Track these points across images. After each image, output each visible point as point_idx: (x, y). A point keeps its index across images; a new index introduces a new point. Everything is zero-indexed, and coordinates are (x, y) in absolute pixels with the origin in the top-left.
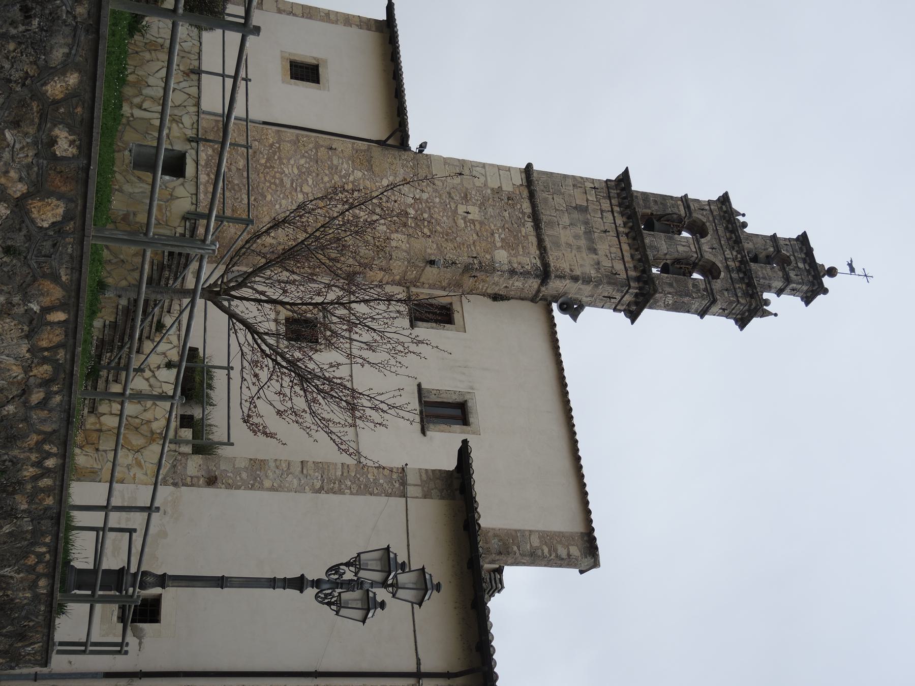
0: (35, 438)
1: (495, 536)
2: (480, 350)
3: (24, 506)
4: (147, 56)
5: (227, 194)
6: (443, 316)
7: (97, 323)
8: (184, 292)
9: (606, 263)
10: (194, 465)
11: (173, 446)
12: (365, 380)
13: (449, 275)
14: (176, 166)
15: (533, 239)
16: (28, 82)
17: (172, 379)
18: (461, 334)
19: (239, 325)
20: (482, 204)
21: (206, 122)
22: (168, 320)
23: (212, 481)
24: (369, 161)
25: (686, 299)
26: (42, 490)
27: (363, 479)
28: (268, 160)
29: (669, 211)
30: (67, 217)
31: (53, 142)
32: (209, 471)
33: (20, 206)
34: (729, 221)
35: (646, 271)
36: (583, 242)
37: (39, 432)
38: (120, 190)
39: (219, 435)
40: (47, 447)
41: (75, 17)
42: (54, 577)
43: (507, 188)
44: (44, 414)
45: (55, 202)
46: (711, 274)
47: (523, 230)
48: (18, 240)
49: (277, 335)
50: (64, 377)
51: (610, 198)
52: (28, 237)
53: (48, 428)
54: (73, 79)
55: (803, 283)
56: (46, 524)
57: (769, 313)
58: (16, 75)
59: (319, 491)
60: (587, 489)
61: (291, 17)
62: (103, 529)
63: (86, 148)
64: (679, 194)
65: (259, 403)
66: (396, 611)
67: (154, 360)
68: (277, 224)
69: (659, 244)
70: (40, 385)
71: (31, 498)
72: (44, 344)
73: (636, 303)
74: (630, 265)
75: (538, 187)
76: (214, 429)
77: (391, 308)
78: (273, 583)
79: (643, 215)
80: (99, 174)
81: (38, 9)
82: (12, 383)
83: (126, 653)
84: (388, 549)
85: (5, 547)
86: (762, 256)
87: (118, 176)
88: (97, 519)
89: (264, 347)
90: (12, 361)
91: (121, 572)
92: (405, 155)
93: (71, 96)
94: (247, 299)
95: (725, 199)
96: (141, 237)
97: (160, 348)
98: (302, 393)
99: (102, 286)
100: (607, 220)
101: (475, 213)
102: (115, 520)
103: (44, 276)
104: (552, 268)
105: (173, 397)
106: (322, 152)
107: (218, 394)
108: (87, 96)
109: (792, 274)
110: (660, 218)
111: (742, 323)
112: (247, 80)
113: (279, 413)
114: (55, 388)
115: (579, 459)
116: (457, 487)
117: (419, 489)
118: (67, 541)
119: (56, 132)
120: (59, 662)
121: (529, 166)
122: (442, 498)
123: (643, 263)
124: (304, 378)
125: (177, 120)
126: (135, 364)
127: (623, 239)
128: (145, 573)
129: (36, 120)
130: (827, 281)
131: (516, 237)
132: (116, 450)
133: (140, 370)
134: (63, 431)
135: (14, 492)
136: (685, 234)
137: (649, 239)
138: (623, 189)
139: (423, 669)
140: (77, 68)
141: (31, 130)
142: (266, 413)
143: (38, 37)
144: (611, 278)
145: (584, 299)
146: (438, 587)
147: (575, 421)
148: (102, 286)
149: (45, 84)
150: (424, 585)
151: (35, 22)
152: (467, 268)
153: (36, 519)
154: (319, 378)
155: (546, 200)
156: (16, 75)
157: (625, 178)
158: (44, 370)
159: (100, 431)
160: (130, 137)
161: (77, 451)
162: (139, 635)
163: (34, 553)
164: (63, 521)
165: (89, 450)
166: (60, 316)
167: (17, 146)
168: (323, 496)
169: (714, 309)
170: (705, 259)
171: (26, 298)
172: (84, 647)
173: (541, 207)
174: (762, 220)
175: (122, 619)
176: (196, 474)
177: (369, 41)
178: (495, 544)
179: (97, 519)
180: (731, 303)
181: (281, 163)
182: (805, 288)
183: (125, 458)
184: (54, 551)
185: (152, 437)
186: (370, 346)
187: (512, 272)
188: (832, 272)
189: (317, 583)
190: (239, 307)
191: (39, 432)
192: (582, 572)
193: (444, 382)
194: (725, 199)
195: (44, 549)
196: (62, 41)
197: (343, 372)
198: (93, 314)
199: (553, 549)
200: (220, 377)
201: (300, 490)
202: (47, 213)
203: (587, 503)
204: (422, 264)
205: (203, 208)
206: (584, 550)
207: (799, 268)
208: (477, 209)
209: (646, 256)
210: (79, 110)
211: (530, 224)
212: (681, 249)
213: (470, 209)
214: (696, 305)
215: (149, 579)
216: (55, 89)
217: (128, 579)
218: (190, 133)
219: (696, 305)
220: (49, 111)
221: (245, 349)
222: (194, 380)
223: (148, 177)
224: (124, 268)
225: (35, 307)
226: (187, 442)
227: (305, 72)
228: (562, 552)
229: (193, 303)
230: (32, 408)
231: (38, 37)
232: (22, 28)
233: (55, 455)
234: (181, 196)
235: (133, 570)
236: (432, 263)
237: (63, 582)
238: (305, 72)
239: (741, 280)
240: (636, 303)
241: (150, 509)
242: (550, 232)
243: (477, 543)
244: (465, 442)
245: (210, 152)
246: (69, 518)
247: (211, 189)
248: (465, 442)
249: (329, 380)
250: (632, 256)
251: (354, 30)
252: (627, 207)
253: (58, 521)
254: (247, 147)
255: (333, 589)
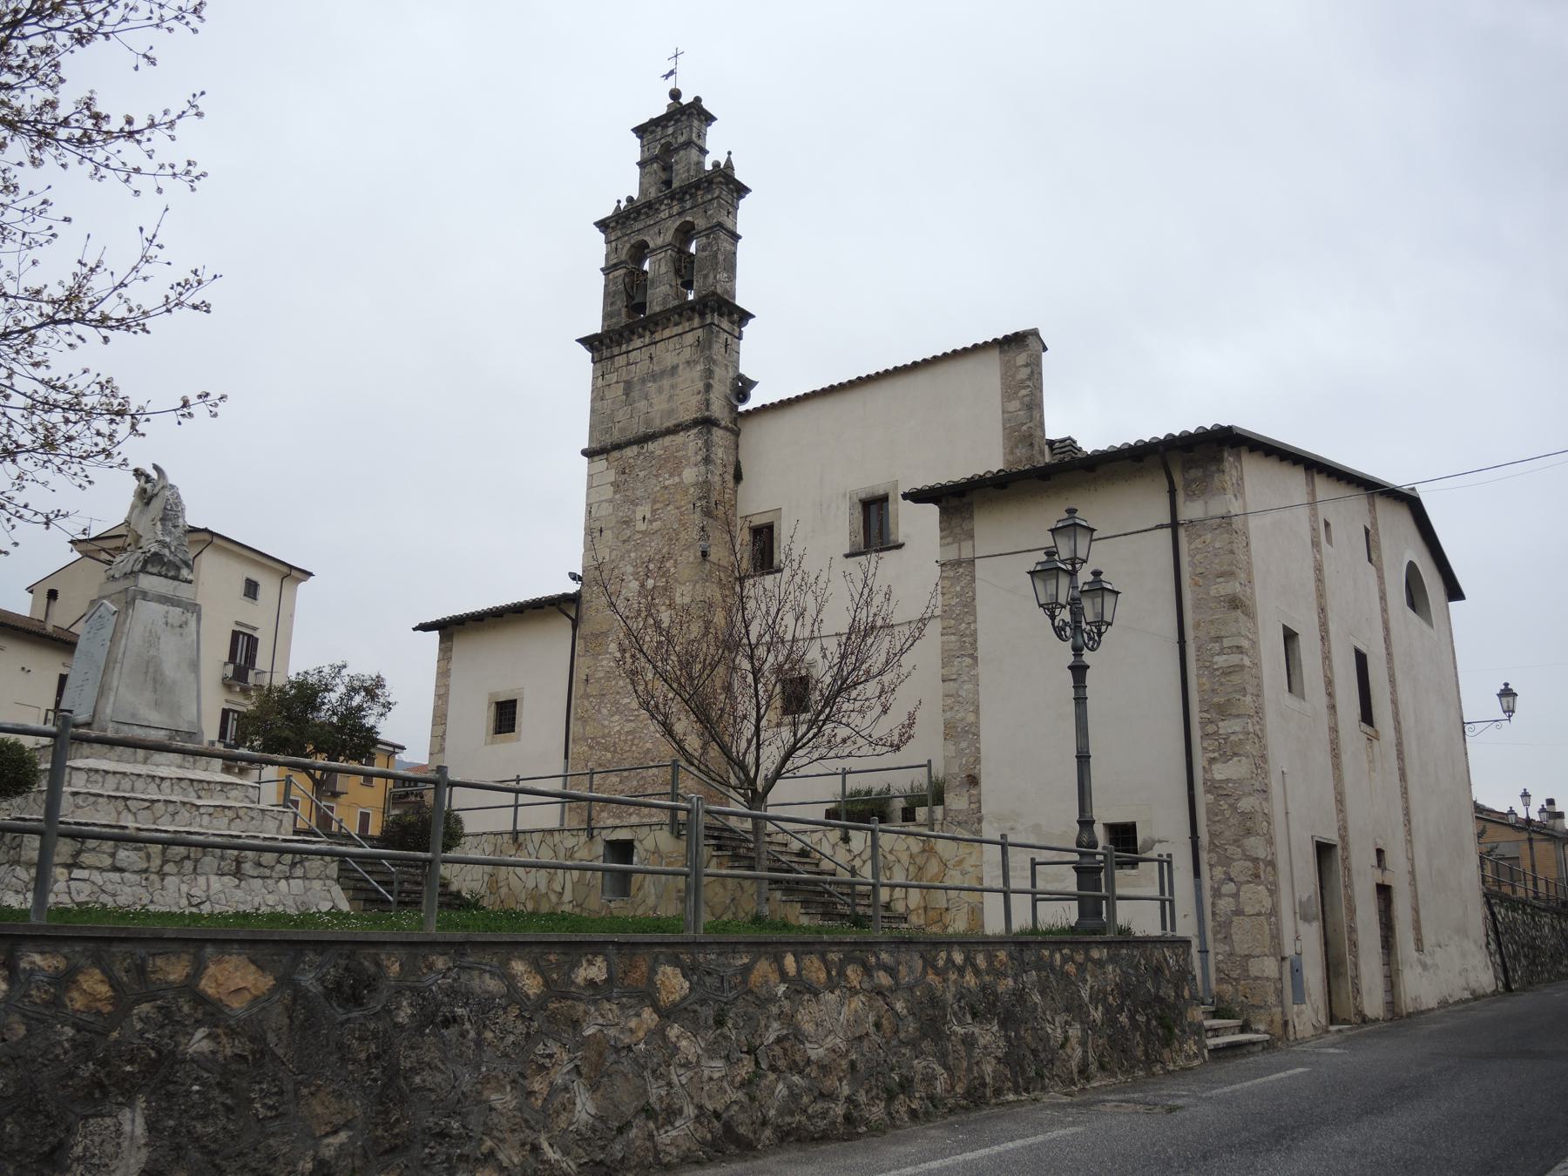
0: (931, 977)
1: (1012, 453)
2: (804, 491)
3: (1010, 982)
4: (504, 890)
5: (649, 791)
6: (764, 535)
7: (805, 921)
8: (757, 829)
9: (687, 353)
10: (956, 801)
11: (937, 827)
12: (837, 620)
13: (718, 534)
14: (622, 850)
15: (668, 440)
16: (527, 1015)
17: (861, 834)
18: (783, 512)
19: (789, 765)
20: (632, 502)
21: (573, 821)
22: (796, 846)
23: (973, 780)
24: (597, 636)
25: (721, 257)
26: (990, 964)
27: (959, 613)
28: (607, 750)
29: (621, 287)
30: (676, 962)
31: (591, 983)
32: (961, 785)
33: (667, 1014)
34: (627, 218)
35: (692, 307)
36: (666, 382)
37: (924, 972)
38: (655, 909)
39: (920, 777)
40: (941, 963)
41: (449, 969)
42: (1088, 943)
43: (611, 476)
44: (903, 969)
45: (660, 976)
46: (688, 232)
47: (658, 452)
48: (707, 1012)
49: (795, 724)
50: (858, 952)
51: (613, 357)
52: (703, 1002)
53: (919, 964)
54: (518, 967)
55: (691, 127)
56: (1029, 956)
57: (729, 161)
58: (521, 1028)
59: (975, 659)
60: (949, 351)
61: (447, 737)
62: (1034, 894)
63: (595, 948)
64: (601, 278)
65: (875, 736)
66: (1101, 557)
67: (842, 856)
68: (668, 730)
69: (659, 296)
70: (871, 976)
71: (1001, 975)
72: (823, 976)
73: (730, 314)
74: (687, 326)
75: (607, 440)
76: (916, 784)
77: (752, 593)
78: (1080, 700)
79: (629, 316)
80: (624, 931)
81: (444, 1009)
82: (871, 1007)
83: (1169, 856)
84: (1032, 573)
85: (1057, 998)
86: (664, 176)
87: (639, 913)
88: (1021, 904)
89: (810, 735)
90: (845, 1008)
91: (1079, 870)
92: (586, 596)
93: (537, 967)
94: (758, 758)
95: (603, 225)
96: (691, 880)
97: (828, 852)
98: (860, 687)
99: (757, 919)
100: (638, 357)
101: (644, 510)
102: (1020, 880)
103: (745, 982)
104: (698, 415)
105: (873, 831)
106: (593, 689)
107: (876, 782)
108: (537, 950)
109: (681, 139)
110: (630, 297)
111: (742, 190)
112: (518, 780)
113: (885, 712)
114: (873, 960)
115: (915, 364)
116: (956, 501)
117: (964, 544)
118: (1049, 932)
119: (580, 980)
120: (1185, 927)
121: (584, 453)
122: (971, 517)
123: (683, 311)
124: (842, 686)
125: (571, 853)
126: (847, 877)
127: (657, 337)
128: (1079, 844)
129: (569, 1002)
130: (685, 100)
131: (666, 460)
132: (946, 889)
133: (853, 872)
134: (922, 947)
135: (995, 994)
136: (646, 267)
137: (655, 307)
138: (601, 343)
139: (1168, 521)
140: (505, 963)
141: (581, 1007)
142: (887, 726)
143: (475, 1008)
144: (703, 346)
145: (731, 374)
146: (1071, 511)
147: (872, 372)
148: (757, 919)
149: (527, 996)
150: (1071, 528)
151: (459, 1011)
152: (707, 513)
153: (1023, 968)
154: (840, 669)
155: (622, 430)
156: (521, 1028)
157: (588, 342)
158: (853, 974)
159: (925, 908)
160: (595, 902)
161: (950, 930)
162: (1150, 845)
163: (1062, 966)
164: (1023, 939)
165: (948, 918)
166: (790, 962)
167: (600, 1021)
168: (980, 654)
169: (729, 225)
170: (673, 243)
171: (773, 999)
172: (1166, 904)
173: (630, 435)
174: (622, 179)
175: (1133, 864)
176: (966, 799)
177: (464, 647)
178: (1021, 452)
179: (1021, 904)
180: (720, 205)
181: (609, 735)
182: (696, 123)
183: (954, 878)
184: (1058, 945)
185: (928, 851)
186: (800, 616)
187: (707, 460)
188: (675, 95)
189: (1077, 651)
190: (769, 764)
191: (924, 972)
192: (1045, 349)
193: (843, 527)
194: (603, 225)
195: (1058, 956)
196: (477, 981)
197: (832, 646)
198: (786, 926)
199: (1021, 385)
200: (854, 783)
201: (975, 680)
202: (673, 983)
203: (965, 349)
204: (708, 566)
205: (664, 817)
206: (1019, 349)
207: (674, 131)
208: (639, 508)
209: (675, 308)
210: (552, 958)
211: (651, 446)
212: (663, 269)
213: (639, 516)
214: (725, 245)
215: (1085, 838)
216: (532, 985)
217: (1087, 862)
218: (583, 837)
219: (725, 245)
220: (557, 990)
221: (816, 755)
222: (861, 811)
223: (636, 878)
224: (728, 894)
225: (782, 988)
226: (931, 812)
227: (505, 716)
228: (1024, 373)
229: (770, 819)
230: (897, 983)
231: (475, 1008)
232: (467, 1026)
233: (949, 954)
234: (656, 844)
235: (1076, 857)
236: (704, 554)
237: (1094, 932)
238: (505, 716)
239: (693, 196)
240: (730, 314)
241: (1004, 845)
242: (657, 422)
243: (1020, 472)
244: (905, 496)
245: (604, 815)
246: (1023, 932)
247: (646, 811)
248: (905, 496)
249: (843, 657)
250: (676, 324)
251: (454, 665)
252: (621, 335)
253: (1023, 944)
254: (592, 773)
255: (1083, 631)
